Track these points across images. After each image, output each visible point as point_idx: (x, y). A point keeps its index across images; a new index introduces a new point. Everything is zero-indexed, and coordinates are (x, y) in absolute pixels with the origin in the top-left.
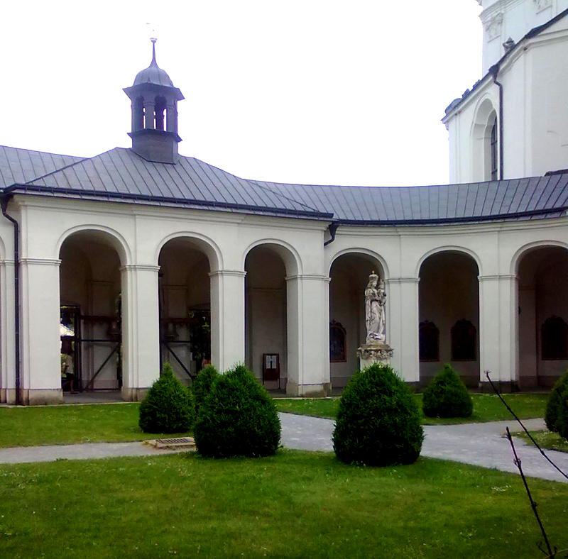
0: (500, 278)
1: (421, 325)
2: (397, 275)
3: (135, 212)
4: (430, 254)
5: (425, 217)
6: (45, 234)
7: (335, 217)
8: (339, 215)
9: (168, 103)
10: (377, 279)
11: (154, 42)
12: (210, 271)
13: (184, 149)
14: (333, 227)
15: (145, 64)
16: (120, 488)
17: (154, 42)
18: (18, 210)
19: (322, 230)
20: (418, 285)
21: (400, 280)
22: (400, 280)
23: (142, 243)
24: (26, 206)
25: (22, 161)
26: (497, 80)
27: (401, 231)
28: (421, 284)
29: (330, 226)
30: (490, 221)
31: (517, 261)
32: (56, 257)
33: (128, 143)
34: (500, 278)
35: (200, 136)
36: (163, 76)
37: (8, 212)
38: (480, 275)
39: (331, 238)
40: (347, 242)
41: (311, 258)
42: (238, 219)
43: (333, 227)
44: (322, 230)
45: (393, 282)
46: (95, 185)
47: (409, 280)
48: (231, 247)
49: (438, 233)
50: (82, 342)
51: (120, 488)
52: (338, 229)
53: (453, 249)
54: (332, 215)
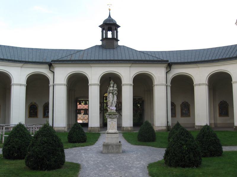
0: (21, 85)
1: (134, 99)
2: (198, 83)
3: (91, 66)
4: (137, 74)
5: (186, 61)
6: (19, 76)
7: (170, 61)
8: (171, 60)
9: (112, 29)
10: (113, 84)
11: (110, 10)
12: (232, 81)
13: (120, 43)
14: (170, 66)
15: (106, 17)
16: (43, 141)
17: (110, 10)
18: (54, 68)
19: (165, 67)
20: (132, 87)
21: (199, 85)
22: (199, 85)
23: (94, 75)
24: (56, 67)
25: (75, 54)
26: (51, 69)
27: (199, 65)
28: (208, 85)
30: (70, 62)
31: (67, 79)
32: (24, 82)
33: (100, 43)
34: (21, 85)
35: (126, 39)
36: (112, 20)
37: (51, 69)
38: (233, 81)
39: (169, 69)
40: (177, 71)
41: (159, 76)
42: (129, 65)
43: (170, 66)
44: (165, 67)
45: (197, 85)
46: (150, 58)
47: (203, 84)
48: (127, 74)
49: (107, 66)
50: (105, 104)
51: (43, 141)
52: (172, 66)
53: (216, 72)
54: (167, 61)
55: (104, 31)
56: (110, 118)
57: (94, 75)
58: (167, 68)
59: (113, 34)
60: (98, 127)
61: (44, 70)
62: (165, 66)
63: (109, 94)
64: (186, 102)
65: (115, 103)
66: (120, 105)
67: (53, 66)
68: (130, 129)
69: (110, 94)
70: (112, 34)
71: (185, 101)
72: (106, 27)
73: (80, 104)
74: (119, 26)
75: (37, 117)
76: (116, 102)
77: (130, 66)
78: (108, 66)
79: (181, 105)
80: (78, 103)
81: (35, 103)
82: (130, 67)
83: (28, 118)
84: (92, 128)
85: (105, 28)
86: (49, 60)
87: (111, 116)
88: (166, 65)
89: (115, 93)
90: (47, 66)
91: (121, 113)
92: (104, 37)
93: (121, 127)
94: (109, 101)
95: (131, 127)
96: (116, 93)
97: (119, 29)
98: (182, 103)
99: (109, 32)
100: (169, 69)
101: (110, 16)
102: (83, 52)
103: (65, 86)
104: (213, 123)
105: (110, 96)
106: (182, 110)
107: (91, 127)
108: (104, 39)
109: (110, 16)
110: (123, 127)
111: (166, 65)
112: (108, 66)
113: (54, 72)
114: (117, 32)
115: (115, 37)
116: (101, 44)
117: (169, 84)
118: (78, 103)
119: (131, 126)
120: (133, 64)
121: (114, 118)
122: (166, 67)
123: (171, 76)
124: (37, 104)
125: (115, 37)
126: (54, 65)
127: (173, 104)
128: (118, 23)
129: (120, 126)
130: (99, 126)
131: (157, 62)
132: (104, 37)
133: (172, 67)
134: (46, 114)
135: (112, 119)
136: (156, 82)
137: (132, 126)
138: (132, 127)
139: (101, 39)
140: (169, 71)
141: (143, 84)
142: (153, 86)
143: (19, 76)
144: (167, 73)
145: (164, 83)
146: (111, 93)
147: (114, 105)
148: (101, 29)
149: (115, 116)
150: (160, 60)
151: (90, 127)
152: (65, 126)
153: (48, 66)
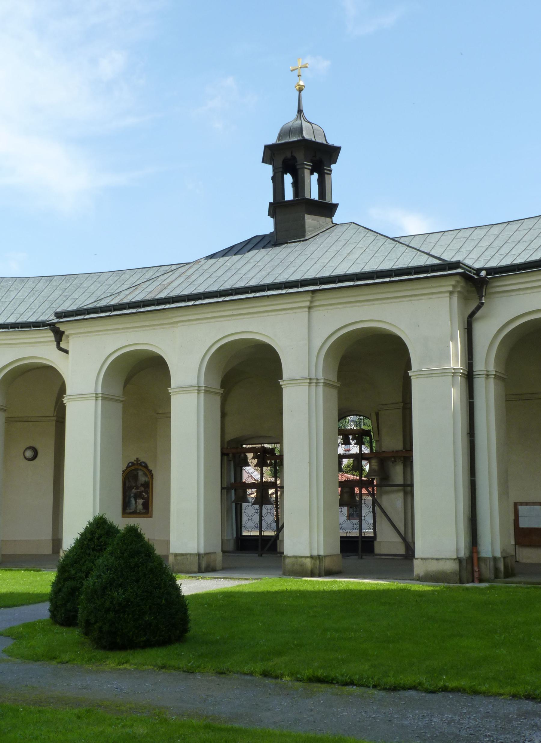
8: (478, 258)
11: (300, 90)
15: (289, 117)
17: (300, 90)
24: (72, 334)
26: (62, 345)
37: (62, 345)
42: (305, 301)
44: (451, 293)
54: (457, 265)
57: (301, 341)
58: (465, 299)
61: (40, 350)
64: (140, 464)
68: (309, 563)
71: (137, 460)
77: (308, 304)
83: (151, 517)
84: (178, 558)
86: (49, 316)
90: (50, 336)
95: (312, 557)
101: (300, 111)
102: (14, 279)
103: (91, 403)
104: (489, 558)
109: (300, 111)
117: (486, 361)
119: (315, 553)
120: (318, 296)
123: (491, 329)
131: (351, 283)
134: (129, 502)
140: (478, 308)
143: (84, 367)
151: (172, 554)
152: (322, 553)
153: (52, 334)
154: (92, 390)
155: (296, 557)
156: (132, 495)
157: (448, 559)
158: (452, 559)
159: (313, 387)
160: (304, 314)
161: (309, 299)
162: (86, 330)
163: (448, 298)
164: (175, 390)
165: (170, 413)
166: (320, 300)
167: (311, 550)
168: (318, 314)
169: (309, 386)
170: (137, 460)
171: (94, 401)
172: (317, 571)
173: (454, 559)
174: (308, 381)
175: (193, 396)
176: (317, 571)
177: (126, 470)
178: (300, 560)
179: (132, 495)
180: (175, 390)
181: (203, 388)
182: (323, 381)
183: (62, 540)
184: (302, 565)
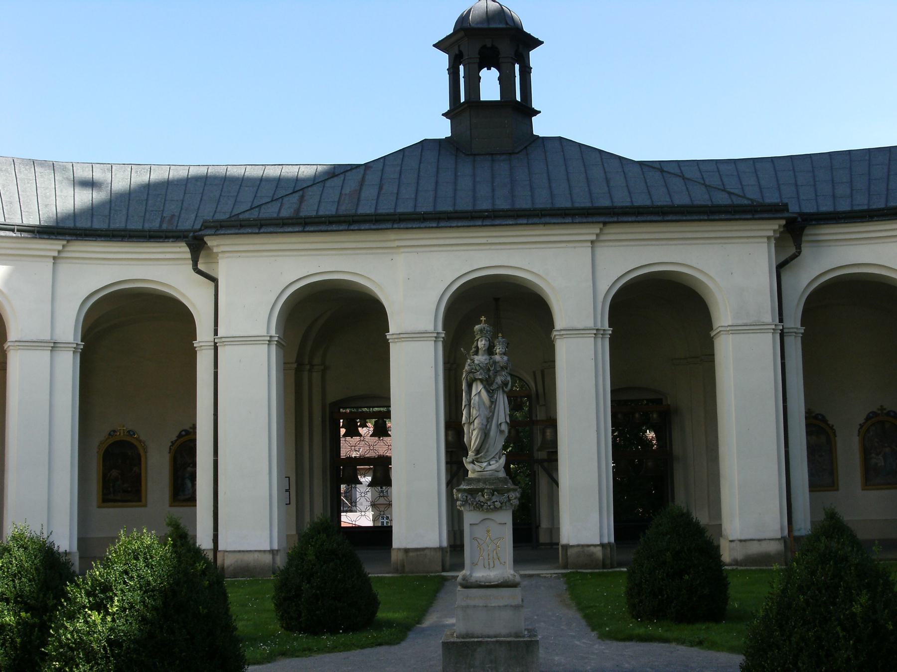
7: (794, 208)
18: (213, 258)
19: (769, 238)
26: (201, 267)
29: (785, 226)
39: (792, 250)
42: (589, 232)
44: (769, 238)
48: (574, 276)
52: (806, 232)
55: (461, 67)
56: (479, 507)
57: (412, 282)
58: (779, 242)
59: (506, 83)
60: (441, 549)
61: (163, 269)
62: (771, 233)
63: (470, 386)
64: (888, 414)
65: (502, 432)
66: (549, 432)
67: (209, 248)
68: (599, 552)
69: (477, 388)
70: (499, 79)
71: (882, 408)
72: (471, 50)
73: (353, 432)
74: (536, 43)
75: (140, 500)
76: (504, 427)
77: (594, 238)
78: (484, 241)
79: (861, 426)
80: (343, 431)
81: (131, 433)
82: (592, 242)
83: (145, 506)
84: (411, 554)
85: (466, 57)
86: (187, 223)
87: (479, 497)
88: (775, 231)
89: (499, 380)
91: (554, 476)
92: (463, 100)
93: (558, 544)
94: (470, 423)
95: (602, 545)
96: (505, 384)
97: (535, 56)
98: (868, 418)
99: (484, 73)
100: (792, 250)
105: (475, 399)
106: (866, 453)
107: (407, 551)
108: (464, 109)
110: (566, 547)
111: (776, 227)
112: (484, 241)
113: (214, 280)
114: (526, 72)
115: (518, 98)
116: (449, 135)
117: (794, 320)
118: (343, 431)
119: (606, 541)
121: (496, 509)
122: (776, 239)
124: (140, 441)
125: (518, 98)
126: (218, 246)
127: (819, 428)
128: (528, 28)
129: (555, 541)
130: (445, 544)
132: (463, 100)
133: (804, 238)
135: (489, 510)
136: (723, 315)
137: (612, 540)
138: (609, 543)
139: (446, 108)
141: (659, 323)
142: (713, 334)
144: (780, 267)
145: (768, 316)
146: (481, 381)
147: (497, 442)
148: (443, 59)
149: (504, 498)
150: (746, 202)
151: (399, 549)
153: (187, 249)
154: (431, 328)
155: (583, 546)
156: (187, 475)
157: (772, 539)
158: (776, 539)
159: (599, 341)
160: (587, 251)
161: (598, 231)
162: (251, 248)
163: (590, 249)
164: (395, 336)
165: (554, 361)
166: (613, 232)
167: (601, 536)
168: (605, 253)
169: (435, 341)
170: (882, 408)
171: (433, 343)
172: (608, 562)
173: (779, 539)
174: (52, 345)
175: (588, 343)
176: (608, 562)
177: (176, 441)
178: (586, 549)
179: (187, 475)
180: (395, 336)
181: (276, 339)
182: (276, 339)
183: (196, 536)
184: (591, 555)
